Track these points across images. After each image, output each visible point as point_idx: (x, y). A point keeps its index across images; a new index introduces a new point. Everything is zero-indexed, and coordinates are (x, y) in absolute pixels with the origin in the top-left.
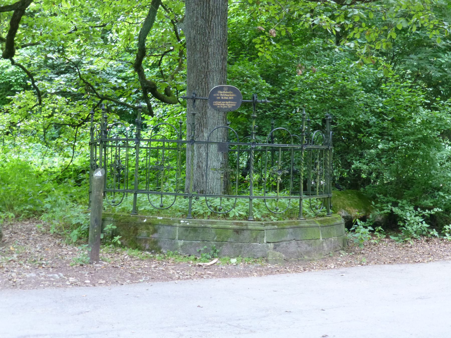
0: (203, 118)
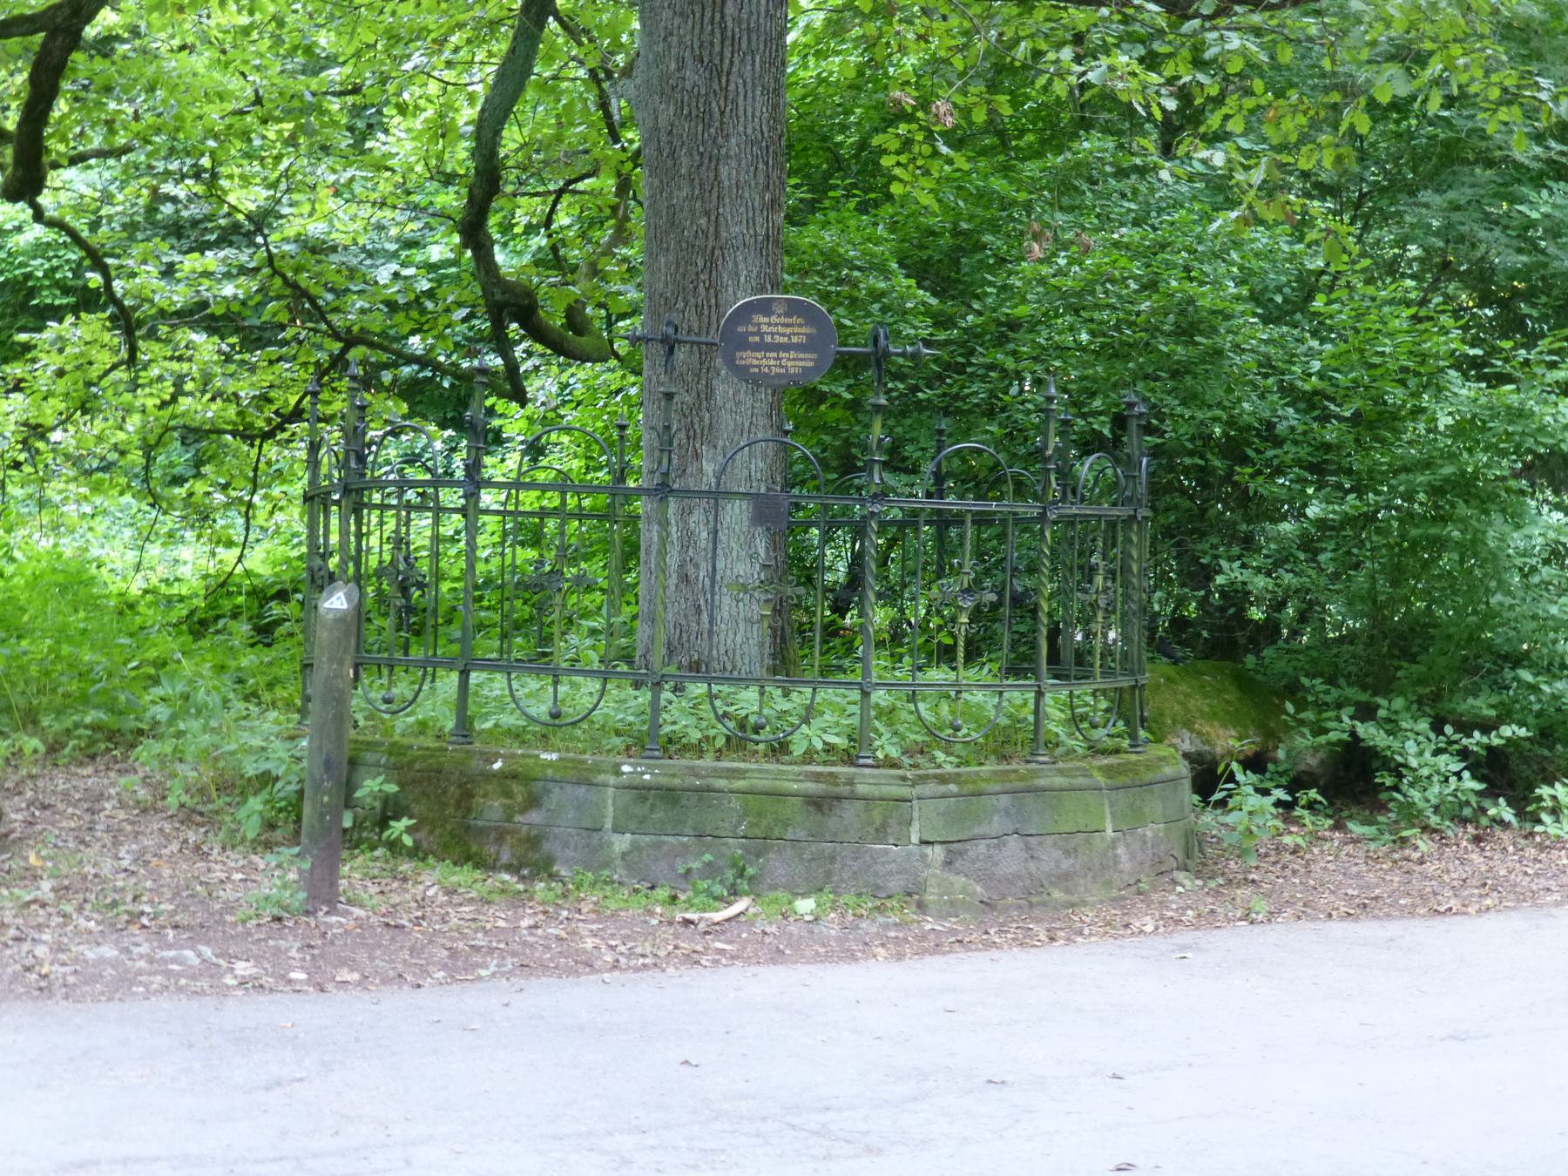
0: (699, 408)
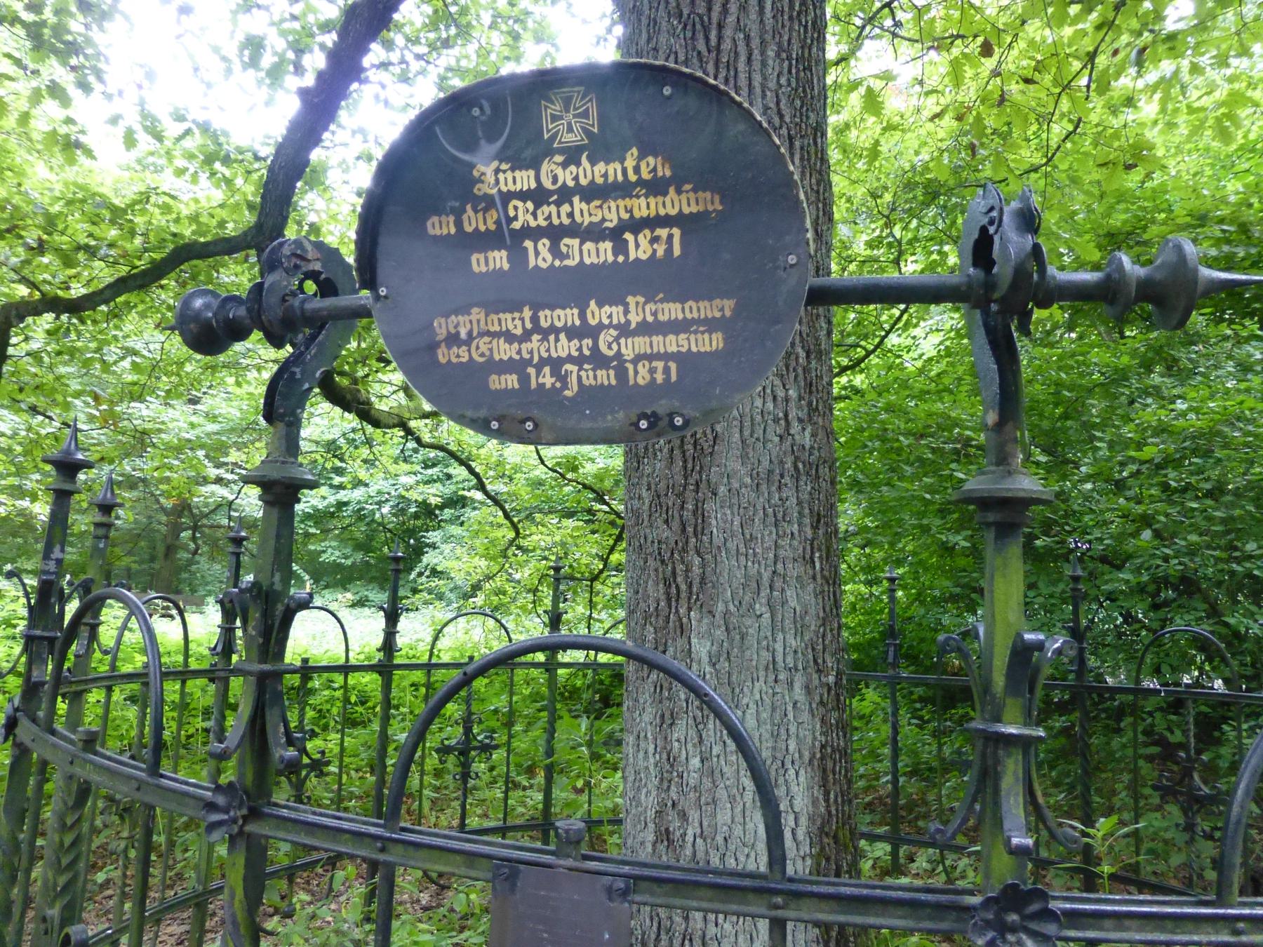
0: (685, 550)
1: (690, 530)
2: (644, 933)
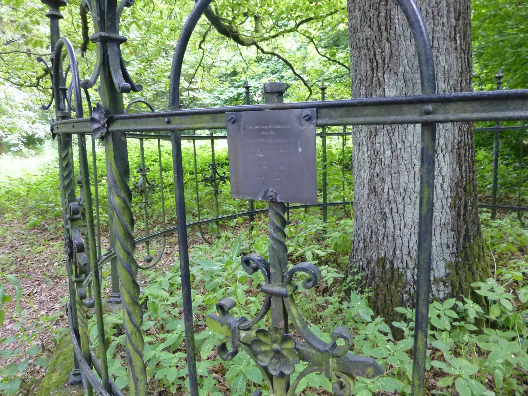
0: (380, 40)
1: (383, 28)
2: (364, 236)
